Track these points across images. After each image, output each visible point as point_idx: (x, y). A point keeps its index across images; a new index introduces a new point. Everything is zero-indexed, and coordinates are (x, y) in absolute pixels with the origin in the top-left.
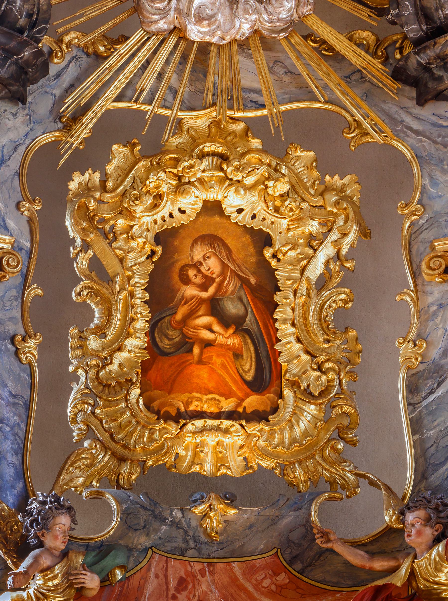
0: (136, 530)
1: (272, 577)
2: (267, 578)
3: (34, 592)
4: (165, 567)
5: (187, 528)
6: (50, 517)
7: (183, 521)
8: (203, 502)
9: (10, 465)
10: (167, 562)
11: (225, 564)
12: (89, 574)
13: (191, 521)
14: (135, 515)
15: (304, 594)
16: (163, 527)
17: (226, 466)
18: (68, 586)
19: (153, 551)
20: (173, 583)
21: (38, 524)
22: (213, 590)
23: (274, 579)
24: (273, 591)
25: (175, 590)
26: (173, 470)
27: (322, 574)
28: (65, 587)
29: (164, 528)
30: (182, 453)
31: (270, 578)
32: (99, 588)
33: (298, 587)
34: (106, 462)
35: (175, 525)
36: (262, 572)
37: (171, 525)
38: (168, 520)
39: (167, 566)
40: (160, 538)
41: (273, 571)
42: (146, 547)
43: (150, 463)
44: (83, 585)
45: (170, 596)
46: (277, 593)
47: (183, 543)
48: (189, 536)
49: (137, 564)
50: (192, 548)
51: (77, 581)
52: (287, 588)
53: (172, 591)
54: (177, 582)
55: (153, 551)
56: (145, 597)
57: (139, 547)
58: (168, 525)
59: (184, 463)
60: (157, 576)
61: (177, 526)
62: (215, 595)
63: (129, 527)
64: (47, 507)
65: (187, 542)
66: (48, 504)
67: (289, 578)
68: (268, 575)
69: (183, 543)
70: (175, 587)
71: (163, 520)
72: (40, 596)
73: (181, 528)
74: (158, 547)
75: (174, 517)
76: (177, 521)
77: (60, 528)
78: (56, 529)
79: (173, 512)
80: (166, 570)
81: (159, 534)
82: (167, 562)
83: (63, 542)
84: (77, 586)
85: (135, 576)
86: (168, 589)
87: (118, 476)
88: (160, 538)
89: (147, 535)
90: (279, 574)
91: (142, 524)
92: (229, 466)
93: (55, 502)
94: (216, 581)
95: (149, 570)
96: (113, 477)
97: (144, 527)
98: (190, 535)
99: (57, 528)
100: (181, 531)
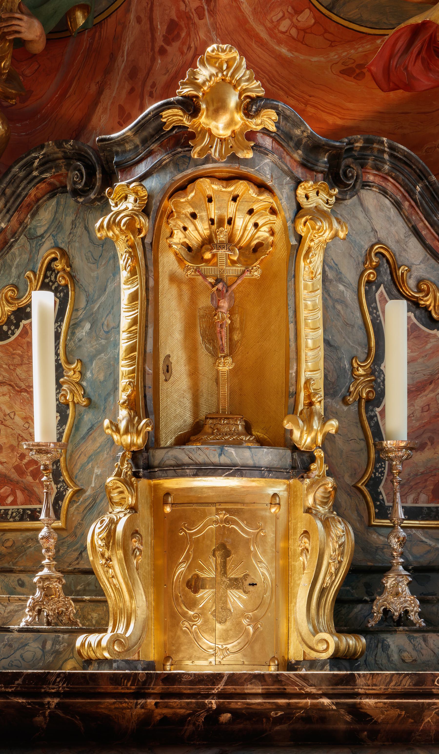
1: (293, 16)
2: (286, 18)
4: (149, 6)
12: (25, 18)
15: (335, 41)
23: (294, 20)
24: (293, 38)
27: (357, 10)
31: (289, 18)
33: (326, 31)
36: (279, 9)
41: (293, 8)
44: (17, 36)
45: (157, 49)
46: (299, 41)
52: (311, 33)
56: (123, 53)
60: (139, 20)
67: (315, 17)
68: (286, 14)
70: (163, 36)
80: (151, 10)
84: (11, 37)
85: (109, 20)
86: (153, 39)
90: (302, 12)
95: (128, 11)
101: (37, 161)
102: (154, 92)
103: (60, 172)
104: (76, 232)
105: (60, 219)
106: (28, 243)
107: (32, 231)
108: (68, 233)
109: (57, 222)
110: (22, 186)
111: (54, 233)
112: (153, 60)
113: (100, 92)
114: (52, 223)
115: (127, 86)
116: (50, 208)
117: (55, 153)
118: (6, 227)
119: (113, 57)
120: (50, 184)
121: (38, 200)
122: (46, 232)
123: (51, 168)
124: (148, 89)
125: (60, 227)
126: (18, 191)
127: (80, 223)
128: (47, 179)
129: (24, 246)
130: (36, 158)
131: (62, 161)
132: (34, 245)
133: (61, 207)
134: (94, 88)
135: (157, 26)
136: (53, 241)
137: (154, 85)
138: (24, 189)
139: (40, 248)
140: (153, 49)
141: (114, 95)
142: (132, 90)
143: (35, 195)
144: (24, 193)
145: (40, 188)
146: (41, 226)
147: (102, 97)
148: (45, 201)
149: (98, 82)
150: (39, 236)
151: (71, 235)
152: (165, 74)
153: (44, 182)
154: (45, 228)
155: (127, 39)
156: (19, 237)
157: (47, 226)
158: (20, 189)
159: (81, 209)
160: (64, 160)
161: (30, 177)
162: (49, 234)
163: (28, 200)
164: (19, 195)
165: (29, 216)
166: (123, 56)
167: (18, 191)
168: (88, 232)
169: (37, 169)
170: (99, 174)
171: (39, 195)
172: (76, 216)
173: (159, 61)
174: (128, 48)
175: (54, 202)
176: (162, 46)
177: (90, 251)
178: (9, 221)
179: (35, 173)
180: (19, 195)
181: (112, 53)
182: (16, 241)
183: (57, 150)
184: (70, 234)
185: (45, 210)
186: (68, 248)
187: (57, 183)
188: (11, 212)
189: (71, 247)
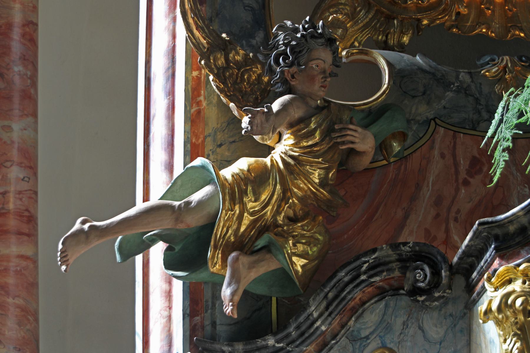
0: (414, 97)
3: (281, 157)
4: (452, 144)
5: (478, 95)
6: (303, 50)
7: (473, 87)
8: (495, 64)
9: (246, 8)
10: (454, 137)
11: (527, 140)
12: (360, 130)
13: (482, 86)
14: (411, 78)
16: (447, 93)
17: (518, 26)
18: (330, 148)
19: (436, 124)
20: (464, 164)
21: (285, 58)
22: (515, 172)
25: (466, 174)
26: (454, 30)
28: (326, 149)
29: (450, 94)
30: (464, 11)
32: (374, 151)
34: (370, 19)
35: (463, 91)
37: (458, 91)
38: (453, 84)
39: (455, 143)
40: (444, 107)
42: (427, 118)
43: (425, 22)
44: (351, 146)
45: (460, 181)
47: (474, 114)
48: (480, 104)
49: (417, 140)
50: (485, 121)
51: (343, 139)
53: (463, 175)
54: (468, 163)
55: (436, 124)
56: (428, 183)
57: (418, 118)
58: (454, 90)
59: (468, 23)
60: (443, 156)
61: (466, 93)
62: (517, 180)
63: (405, 92)
64: (299, 35)
65: (479, 113)
66: (300, 32)
69: (474, 114)
70: (466, 170)
71: (447, 85)
72: (290, 160)
73: (471, 96)
74: (442, 119)
75: (460, 81)
76: (465, 86)
77: (318, 66)
78: (312, 67)
79: (459, 75)
80: (454, 147)
81: (443, 102)
82: (454, 137)
83: (322, 86)
84: (344, 147)
85: (414, 155)
86: (457, 172)
87: (387, 37)
88: (444, 107)
89: (428, 103)
91: (421, 89)
92: (521, 26)
93: (309, 28)
94: (517, 162)
95: (432, 148)
96: (380, 37)
97: (424, 93)
98: (482, 103)
99: (314, 66)
100: (471, 99)
101: (366, 265)
102: (459, 217)
103: (392, 275)
104: (408, 332)
105: (389, 320)
106: (351, 345)
107: (355, 333)
108: (398, 333)
109: (384, 325)
110: (348, 290)
111: (382, 334)
112: (457, 190)
113: (406, 217)
114: (379, 325)
115: (433, 212)
116: (378, 311)
117: (388, 256)
118: (326, 330)
119: (418, 187)
120: (378, 288)
121: (364, 303)
122: (372, 333)
123: (382, 271)
124: (453, 214)
125: (389, 328)
126: (343, 295)
127: (413, 324)
128: (375, 283)
129: (345, 347)
130: (365, 262)
131: (396, 264)
132: (357, 347)
133: (391, 310)
134: (400, 214)
135: (460, 161)
136: (379, 342)
137: (458, 211)
138: (349, 293)
139: (364, 349)
140: (457, 180)
141: (420, 219)
142: (437, 216)
143: (360, 299)
144: (350, 297)
145: (366, 291)
146: (365, 329)
147: (408, 221)
148: (372, 304)
149: (404, 208)
150: (364, 338)
151: (402, 335)
152: (469, 202)
153: (372, 286)
154: (371, 330)
155: (432, 172)
156: (340, 339)
157: (373, 328)
158: (345, 293)
159: (414, 310)
160: (398, 263)
161: (358, 281)
162: (375, 335)
163: (352, 304)
164: (344, 299)
165: (353, 319)
166: (428, 186)
167: (343, 295)
168: (423, 331)
169: (365, 273)
170: (445, 272)
171: (365, 298)
172: (409, 317)
173: (463, 191)
174: (433, 180)
175: (382, 304)
176: (465, 178)
177: (425, 349)
178: (330, 324)
179: (363, 277)
180: (344, 299)
181: (418, 184)
182: (337, 343)
183: (390, 252)
184: (401, 334)
185: (372, 313)
186: (398, 348)
187: (387, 287)
188: (333, 316)
189: (402, 346)
